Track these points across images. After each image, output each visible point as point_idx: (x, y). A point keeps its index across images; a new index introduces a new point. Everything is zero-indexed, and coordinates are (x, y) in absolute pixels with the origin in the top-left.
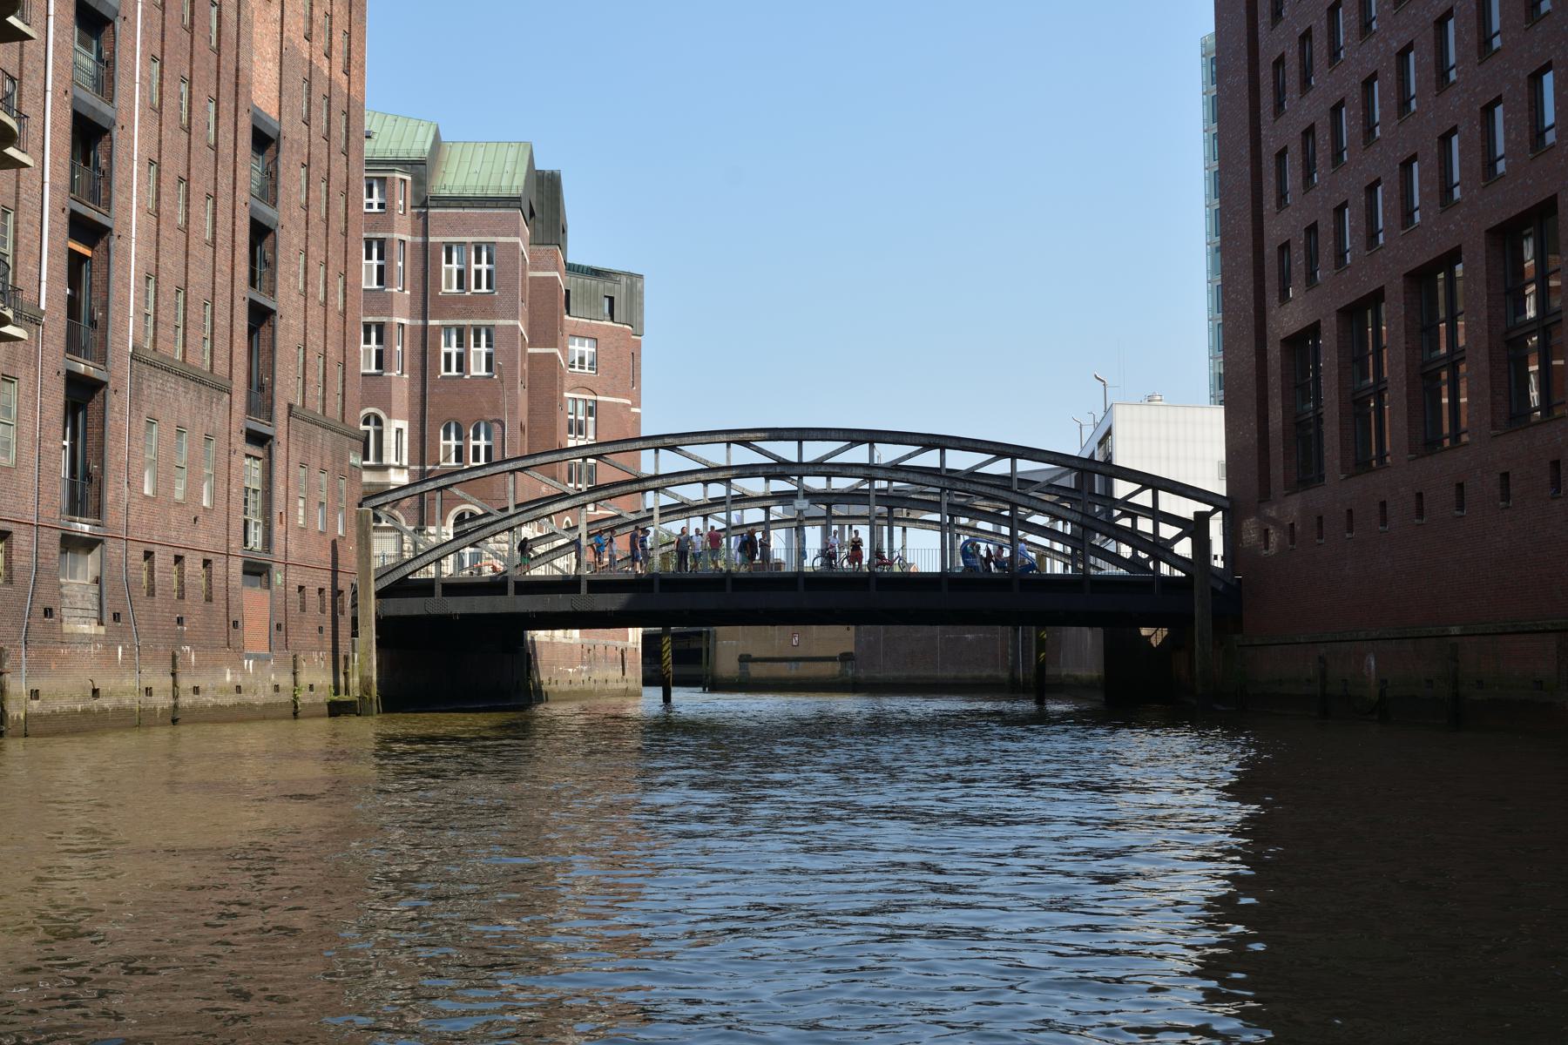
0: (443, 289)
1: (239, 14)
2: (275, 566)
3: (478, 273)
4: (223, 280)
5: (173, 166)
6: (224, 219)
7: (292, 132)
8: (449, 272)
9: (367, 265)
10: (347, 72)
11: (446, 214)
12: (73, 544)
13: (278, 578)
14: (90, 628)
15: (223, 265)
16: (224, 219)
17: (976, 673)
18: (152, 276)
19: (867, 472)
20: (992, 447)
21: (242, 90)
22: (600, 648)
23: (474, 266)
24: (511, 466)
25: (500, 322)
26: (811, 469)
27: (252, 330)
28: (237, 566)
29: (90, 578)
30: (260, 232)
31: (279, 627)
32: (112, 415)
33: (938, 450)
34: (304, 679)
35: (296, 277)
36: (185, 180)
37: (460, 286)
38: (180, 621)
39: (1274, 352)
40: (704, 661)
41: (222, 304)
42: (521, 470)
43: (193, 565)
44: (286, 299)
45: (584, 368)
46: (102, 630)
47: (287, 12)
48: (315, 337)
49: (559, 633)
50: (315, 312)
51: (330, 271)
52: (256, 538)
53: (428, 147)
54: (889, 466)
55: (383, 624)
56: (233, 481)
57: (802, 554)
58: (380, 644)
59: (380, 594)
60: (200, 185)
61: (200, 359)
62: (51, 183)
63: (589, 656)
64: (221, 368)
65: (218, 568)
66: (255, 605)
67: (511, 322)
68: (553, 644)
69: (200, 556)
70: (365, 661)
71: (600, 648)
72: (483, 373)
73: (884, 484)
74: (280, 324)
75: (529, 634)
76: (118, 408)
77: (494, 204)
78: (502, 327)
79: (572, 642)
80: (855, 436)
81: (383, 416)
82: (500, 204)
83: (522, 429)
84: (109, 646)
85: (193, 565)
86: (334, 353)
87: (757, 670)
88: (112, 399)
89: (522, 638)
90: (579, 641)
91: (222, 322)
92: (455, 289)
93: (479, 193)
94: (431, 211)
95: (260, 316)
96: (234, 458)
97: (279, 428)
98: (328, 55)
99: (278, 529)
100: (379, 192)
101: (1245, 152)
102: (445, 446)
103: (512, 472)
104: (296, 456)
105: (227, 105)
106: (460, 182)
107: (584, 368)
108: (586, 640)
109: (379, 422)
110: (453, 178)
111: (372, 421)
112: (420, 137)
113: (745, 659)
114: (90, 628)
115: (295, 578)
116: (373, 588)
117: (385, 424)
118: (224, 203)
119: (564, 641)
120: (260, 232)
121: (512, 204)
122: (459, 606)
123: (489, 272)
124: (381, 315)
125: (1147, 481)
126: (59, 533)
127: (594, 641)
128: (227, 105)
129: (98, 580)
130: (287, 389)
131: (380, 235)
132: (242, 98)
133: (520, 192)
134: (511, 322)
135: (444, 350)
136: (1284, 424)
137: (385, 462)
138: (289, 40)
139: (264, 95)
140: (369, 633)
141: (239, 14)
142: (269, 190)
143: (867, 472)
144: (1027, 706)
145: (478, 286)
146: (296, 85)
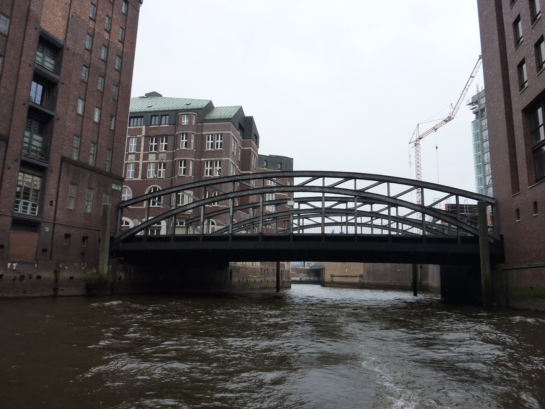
0: (206, 149)
3: (217, 143)
8: (208, 143)
9: (182, 142)
11: (208, 125)
17: (377, 282)
19: (321, 189)
20: (375, 177)
23: (216, 141)
25: (223, 159)
26: (297, 189)
33: (354, 180)
37: (211, 148)
54: (331, 186)
57: (421, 267)
67: (227, 159)
68: (246, 268)
73: (530, 320)
75: (232, 264)
77: (223, 121)
78: (224, 160)
80: (316, 174)
82: (225, 121)
87: (336, 279)
90: (260, 267)
92: (210, 149)
94: (204, 124)
101: (496, 37)
102: (151, 145)
106: (219, 115)
113: (332, 276)
121: (229, 120)
123: (221, 143)
124: (185, 157)
125: (452, 191)
127: (268, 267)
134: (227, 159)
135: (206, 168)
136: (526, 152)
143: (321, 189)
145: (217, 147)
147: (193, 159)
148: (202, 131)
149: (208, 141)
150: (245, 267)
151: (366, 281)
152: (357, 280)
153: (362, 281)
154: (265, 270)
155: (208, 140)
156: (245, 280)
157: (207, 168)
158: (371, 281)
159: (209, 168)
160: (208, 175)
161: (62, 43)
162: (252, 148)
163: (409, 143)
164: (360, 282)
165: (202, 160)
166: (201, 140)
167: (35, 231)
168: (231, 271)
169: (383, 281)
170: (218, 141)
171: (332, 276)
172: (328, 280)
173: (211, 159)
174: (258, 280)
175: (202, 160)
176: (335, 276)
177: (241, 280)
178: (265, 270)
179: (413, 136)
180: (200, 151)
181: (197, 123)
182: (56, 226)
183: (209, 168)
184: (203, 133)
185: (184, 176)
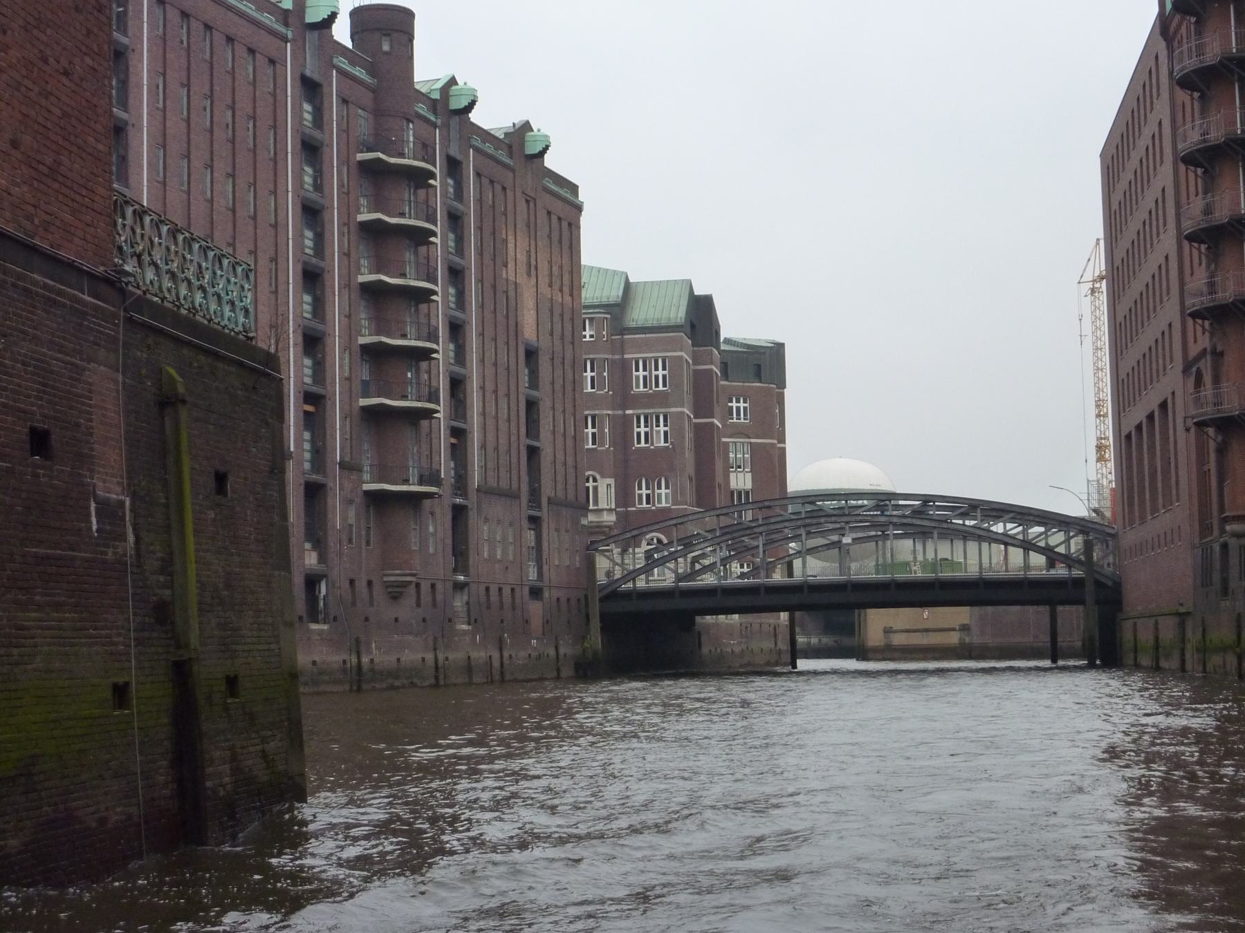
1: (516, 292)
2: (545, 589)
3: (657, 377)
4: (513, 438)
5: (489, 386)
6: (513, 406)
7: (544, 344)
8: (638, 377)
10: (571, 295)
12: (459, 587)
13: (546, 594)
14: (465, 627)
15: (514, 431)
16: (513, 406)
18: (483, 446)
20: (964, 501)
21: (519, 334)
22: (756, 627)
23: (654, 373)
24: (674, 522)
25: (673, 410)
27: (529, 459)
28: (526, 590)
29: (464, 602)
30: (531, 405)
31: (547, 622)
32: (471, 522)
34: (562, 651)
35: (549, 425)
36: (495, 392)
37: (645, 386)
38: (502, 621)
39: (1123, 438)
40: (857, 633)
41: (514, 452)
42: (680, 524)
43: (507, 591)
44: (545, 442)
45: (740, 419)
46: (470, 628)
47: (540, 279)
48: (560, 457)
49: (722, 617)
50: (560, 439)
51: (567, 415)
52: (532, 574)
53: (621, 293)
55: (604, 617)
56: (523, 544)
58: (603, 630)
59: (601, 600)
60: (502, 390)
61: (504, 484)
62: (143, 22)
63: (746, 633)
64: (515, 486)
65: (518, 590)
66: (536, 609)
67: (679, 409)
68: (718, 624)
69: (509, 587)
70: (596, 640)
71: (756, 627)
72: (662, 444)
74: (543, 454)
75: (698, 619)
76: (473, 517)
79: (732, 622)
81: (598, 477)
83: (691, 479)
84: (473, 634)
85: (507, 591)
86: (570, 461)
87: (898, 640)
88: (471, 513)
89: (693, 623)
91: (514, 460)
92: (641, 388)
93: (655, 323)
94: (625, 337)
95: (533, 452)
96: (523, 533)
97: (544, 513)
98: (561, 291)
99: (545, 568)
100: (589, 324)
103: (676, 525)
104: (553, 526)
105: (512, 343)
106: (642, 317)
107: (740, 419)
108: (744, 620)
109: (595, 480)
110: (640, 314)
111: (591, 479)
112: (615, 285)
113: (888, 631)
114: (465, 627)
115: (555, 594)
116: (598, 597)
117: (599, 481)
118: (513, 396)
119: (727, 621)
120: (531, 405)
122: (646, 606)
126: (452, 584)
128: (512, 343)
129: (468, 603)
130: (547, 491)
131: (591, 356)
132: (519, 338)
133: (683, 320)
134: (679, 409)
135: (636, 430)
137: (600, 507)
138: (541, 293)
139: (529, 332)
140: (596, 624)
141: (516, 292)
142: (534, 383)
144: (1047, 663)
145: (657, 386)
146: (545, 314)
147: (609, 412)
148: (623, 354)
149: (637, 373)
150: (717, 625)
151: (975, 639)
152: (954, 639)
153: (967, 640)
154: (746, 628)
155: (637, 370)
156: (719, 650)
157: (638, 430)
158: (989, 640)
159: (643, 430)
160: (643, 444)
161: (536, 345)
162: (714, 368)
163: (1079, 283)
164: (962, 644)
165: (629, 412)
166: (622, 371)
167: (538, 600)
168: (699, 633)
169: (1018, 639)
170: (657, 373)
171: (888, 631)
172: (877, 644)
173: (646, 411)
174: (737, 650)
175: (629, 412)
176: (896, 632)
177: (713, 650)
178: (746, 628)
179: (1086, 267)
180: (623, 396)
181: (612, 335)
182: (1045, 639)
183: (643, 430)
184: (626, 356)
185: (596, 449)
